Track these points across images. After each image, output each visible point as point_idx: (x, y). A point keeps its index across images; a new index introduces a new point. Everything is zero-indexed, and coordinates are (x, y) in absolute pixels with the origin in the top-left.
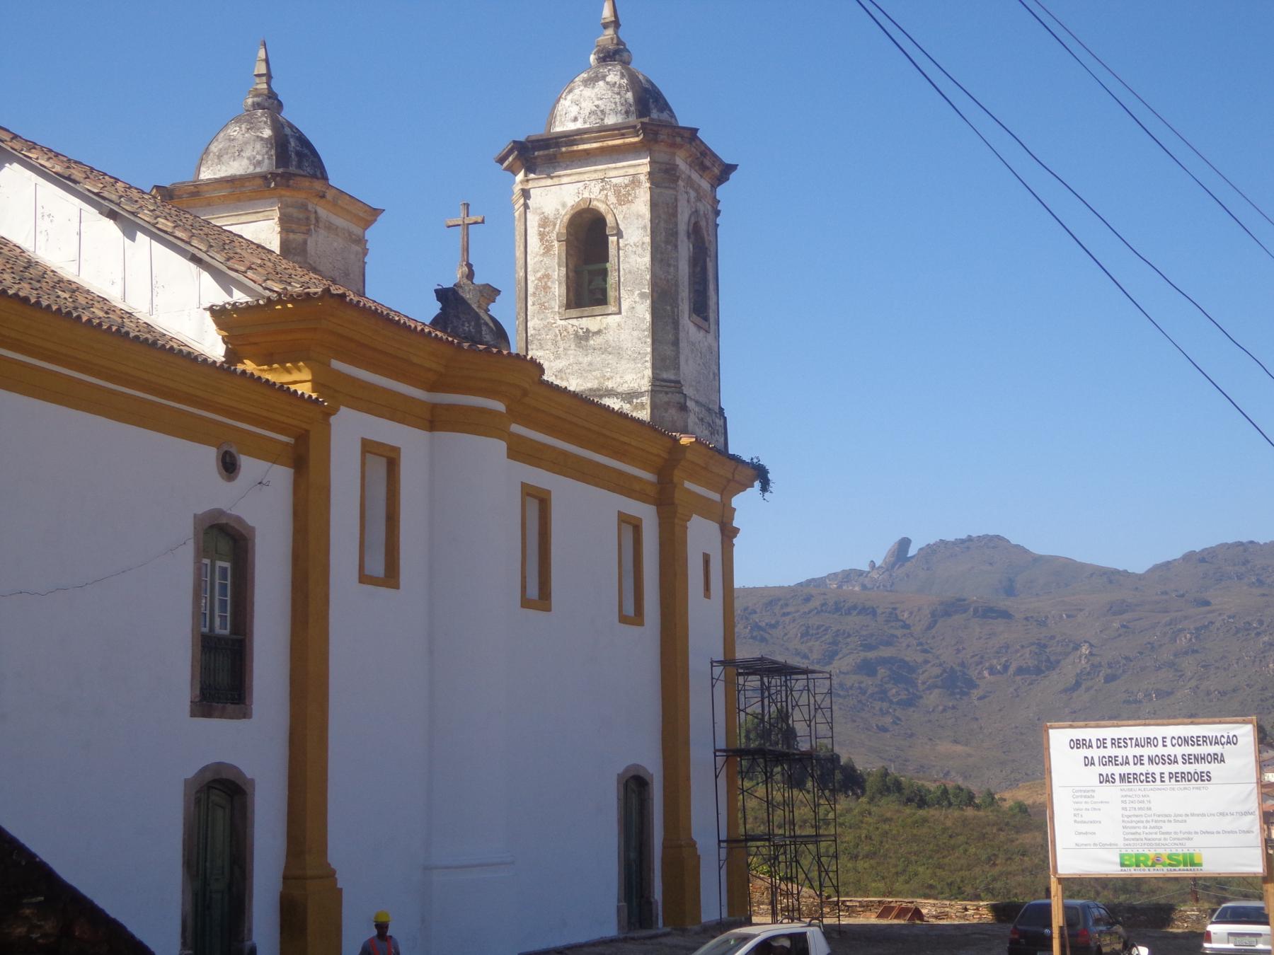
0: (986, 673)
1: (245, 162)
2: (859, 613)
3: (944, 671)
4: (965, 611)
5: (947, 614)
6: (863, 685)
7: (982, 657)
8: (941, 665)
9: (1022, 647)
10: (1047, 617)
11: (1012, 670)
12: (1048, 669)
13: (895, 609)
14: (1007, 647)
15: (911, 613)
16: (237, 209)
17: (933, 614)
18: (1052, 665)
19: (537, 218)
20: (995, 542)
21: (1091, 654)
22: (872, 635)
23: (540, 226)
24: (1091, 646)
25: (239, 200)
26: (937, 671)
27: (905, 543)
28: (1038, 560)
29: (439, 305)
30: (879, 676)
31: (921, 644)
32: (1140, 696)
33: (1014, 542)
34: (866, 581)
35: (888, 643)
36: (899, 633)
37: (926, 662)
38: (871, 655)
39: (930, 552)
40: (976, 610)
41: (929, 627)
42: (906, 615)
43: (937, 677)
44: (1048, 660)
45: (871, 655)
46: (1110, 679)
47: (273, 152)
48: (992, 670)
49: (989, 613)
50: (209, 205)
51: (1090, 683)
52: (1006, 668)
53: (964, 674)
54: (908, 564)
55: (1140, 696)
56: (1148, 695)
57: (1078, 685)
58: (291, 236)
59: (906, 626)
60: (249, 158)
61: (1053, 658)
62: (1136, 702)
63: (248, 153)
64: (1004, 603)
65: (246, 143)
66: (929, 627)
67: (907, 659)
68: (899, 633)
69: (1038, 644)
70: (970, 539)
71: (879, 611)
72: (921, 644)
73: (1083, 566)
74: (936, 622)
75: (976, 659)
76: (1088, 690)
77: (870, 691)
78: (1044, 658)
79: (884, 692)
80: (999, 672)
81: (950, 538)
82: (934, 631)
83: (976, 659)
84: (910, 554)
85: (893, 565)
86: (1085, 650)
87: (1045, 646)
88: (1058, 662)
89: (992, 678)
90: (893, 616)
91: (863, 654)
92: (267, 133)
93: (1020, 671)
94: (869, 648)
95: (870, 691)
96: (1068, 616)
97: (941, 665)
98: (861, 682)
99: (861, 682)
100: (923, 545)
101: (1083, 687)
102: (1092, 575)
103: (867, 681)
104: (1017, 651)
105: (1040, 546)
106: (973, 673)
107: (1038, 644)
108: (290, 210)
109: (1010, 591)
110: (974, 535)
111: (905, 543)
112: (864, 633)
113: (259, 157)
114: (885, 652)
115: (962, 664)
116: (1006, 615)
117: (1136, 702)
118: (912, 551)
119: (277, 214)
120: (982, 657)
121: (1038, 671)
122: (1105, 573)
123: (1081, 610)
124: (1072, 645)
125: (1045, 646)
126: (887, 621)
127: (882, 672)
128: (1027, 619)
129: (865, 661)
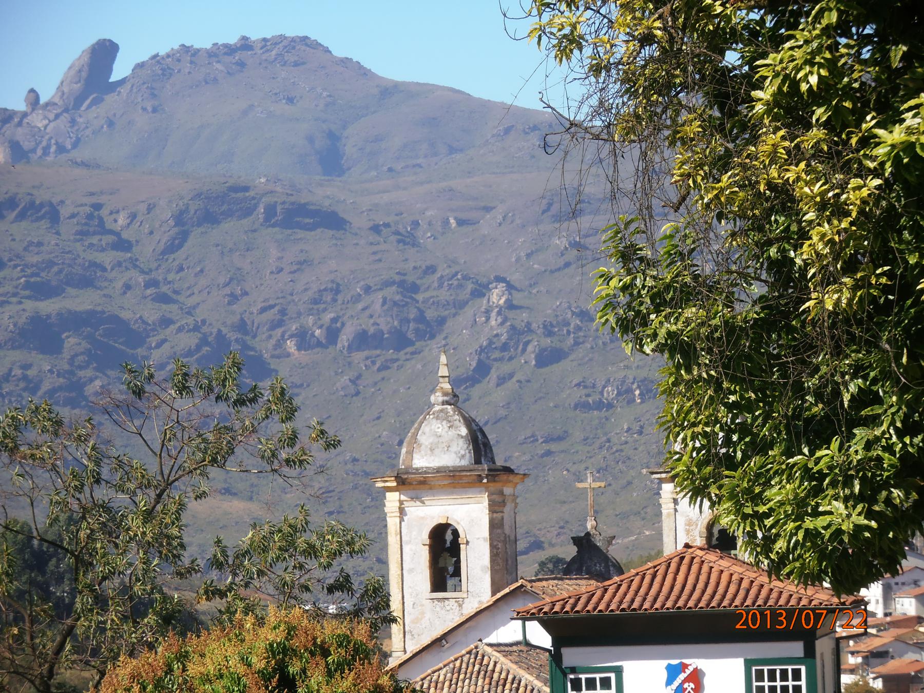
0: (291, 345)
1: (453, 456)
2: (22, 216)
3: (204, 341)
4: (248, 212)
5: (209, 218)
6: (31, 373)
7: (283, 312)
8: (196, 328)
9: (368, 289)
10: (416, 224)
11: (344, 339)
12: (420, 335)
13: (98, 207)
14: (337, 291)
15: (133, 216)
16: (452, 494)
17: (179, 218)
18: (430, 329)
19: (684, 519)
20: (298, 51)
21: (510, 305)
22: (50, 264)
23: (686, 525)
24: (510, 287)
25: (455, 487)
26: (189, 341)
27: (104, 53)
28: (391, 92)
29: (575, 549)
30: (66, 355)
31: (153, 283)
32: (610, 392)
33: (338, 51)
34: (20, 134)
35: (86, 280)
36: (107, 258)
37: (166, 322)
38: (49, 307)
39: (160, 70)
40: (270, 211)
41: (172, 247)
42: (122, 220)
43: (189, 353)
44: (421, 318)
45: (49, 307)
46: (547, 358)
47: (471, 447)
48: (304, 340)
49: (300, 217)
50: (431, 489)
51: (506, 368)
52: (333, 335)
53: (246, 347)
54: (110, 98)
55: (610, 392)
56: (625, 393)
57: (482, 369)
58: (495, 515)
59: (122, 245)
60: (456, 453)
61: (430, 314)
62: (599, 405)
63: (454, 448)
64: (323, 193)
65: (452, 440)
66: (172, 247)
67: (125, 315)
68: (107, 258)
69: (401, 284)
70: (245, 44)
71: (64, 212)
72: (153, 283)
73: (484, 108)
74: (183, 236)
75: (271, 314)
76: (502, 381)
77: (46, 386)
78: (413, 314)
79: (77, 387)
80: (319, 344)
81: (203, 42)
82: (181, 254)
83: (271, 314)
84: (114, 78)
85: (79, 100)
86: (497, 296)
87: (415, 288)
88: (442, 321)
89: (303, 357)
90: (94, 223)
91: (29, 305)
92: (464, 431)
93: (363, 340)
94: (42, 291)
95: (46, 386)
96: (461, 223)
97: (196, 328)
98: (26, 367)
99: (26, 367)
100: (144, 56)
101: (494, 375)
102: (507, 131)
103: (42, 363)
104: (357, 299)
105: (392, 64)
106: (264, 346)
107: (401, 284)
108: (494, 497)
109: (331, 161)
110: (255, 35)
111: (104, 53)
112: (35, 259)
113: (463, 452)
114: (81, 301)
115: (242, 327)
116: (332, 221)
117: (599, 405)
118: (121, 69)
119: (486, 503)
120: (283, 312)
121: (400, 341)
122: (535, 128)
123: (488, 209)
124: (470, 286)
125: (415, 288)
126: (83, 234)
127: (72, 342)
128: (376, 229)
129: (37, 321)
